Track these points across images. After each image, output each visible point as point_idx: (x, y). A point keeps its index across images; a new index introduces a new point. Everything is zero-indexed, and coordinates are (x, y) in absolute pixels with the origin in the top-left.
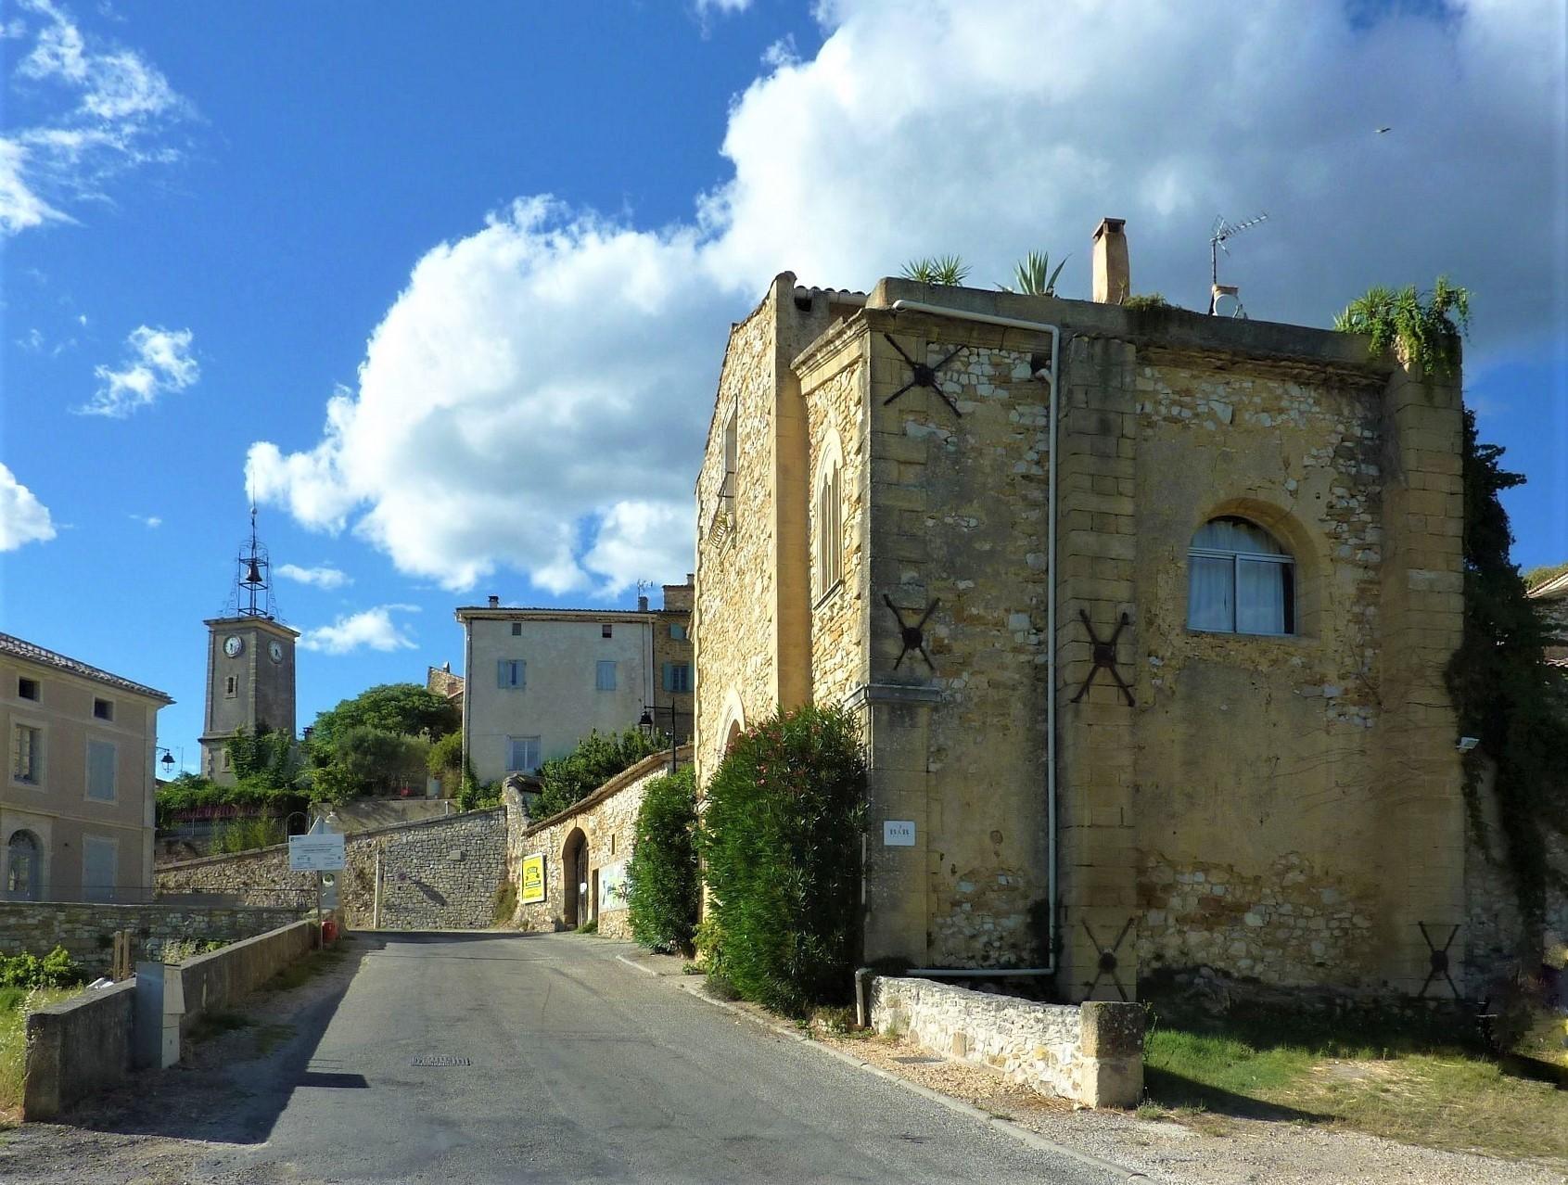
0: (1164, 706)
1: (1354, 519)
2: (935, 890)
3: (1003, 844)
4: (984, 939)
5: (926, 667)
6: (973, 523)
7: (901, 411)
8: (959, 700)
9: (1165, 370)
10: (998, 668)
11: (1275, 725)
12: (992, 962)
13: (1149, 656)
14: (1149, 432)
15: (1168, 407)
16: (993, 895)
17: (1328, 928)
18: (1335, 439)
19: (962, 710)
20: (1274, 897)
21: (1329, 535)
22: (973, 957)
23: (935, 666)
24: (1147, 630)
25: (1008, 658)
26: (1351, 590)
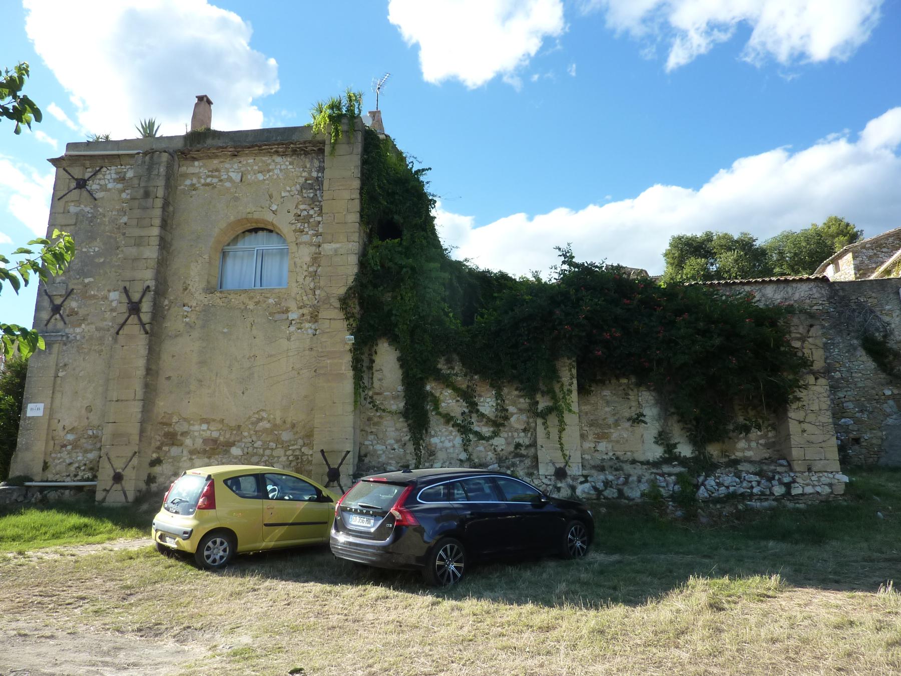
0: (188, 332)
1: (311, 220)
2: (53, 439)
3: (92, 413)
4: (77, 465)
5: (62, 323)
6: (97, 249)
7: (66, 202)
8: (78, 339)
9: (205, 161)
10: (101, 320)
11: (255, 338)
12: (79, 478)
13: (184, 306)
14: (194, 192)
15: (205, 179)
16: (83, 441)
17: (285, 455)
18: (302, 180)
19: (79, 343)
20: (250, 437)
21: (295, 231)
22: (69, 476)
23: (67, 322)
24: (183, 293)
25: (108, 315)
26: (308, 259)
